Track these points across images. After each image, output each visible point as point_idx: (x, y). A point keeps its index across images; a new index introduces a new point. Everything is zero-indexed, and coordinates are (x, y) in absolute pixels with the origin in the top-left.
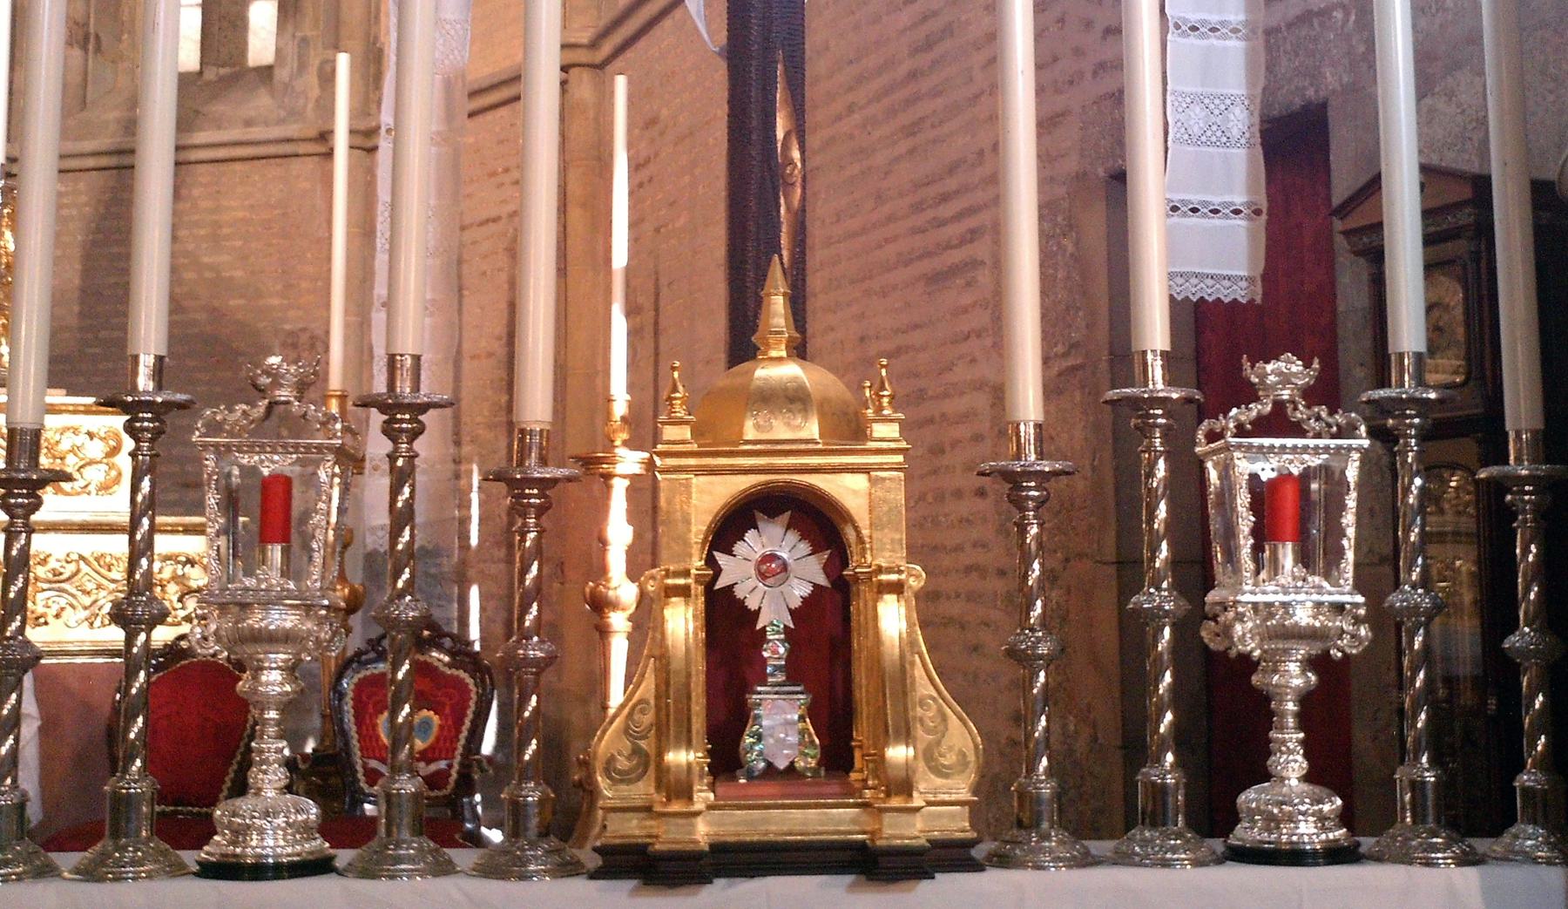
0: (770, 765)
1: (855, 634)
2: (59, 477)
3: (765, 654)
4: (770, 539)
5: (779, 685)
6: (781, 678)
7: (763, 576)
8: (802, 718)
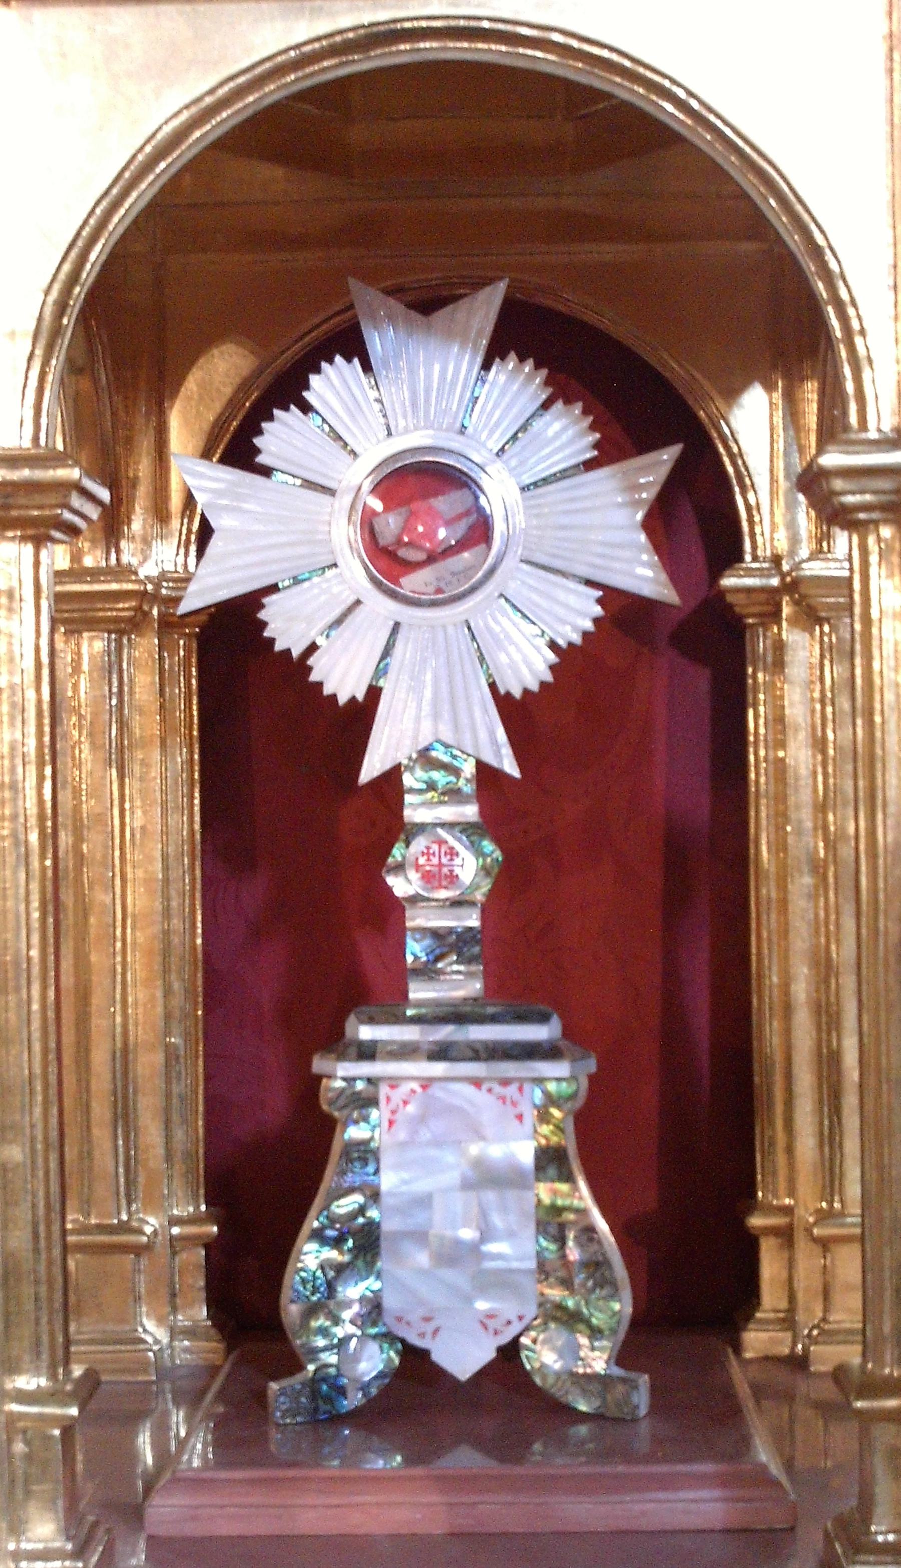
0: (415, 1363)
1: (761, 815)
2: (553, 645)
3: (401, 886)
4: (428, 391)
5: (456, 1015)
6: (461, 983)
7: (388, 561)
8: (550, 1160)
